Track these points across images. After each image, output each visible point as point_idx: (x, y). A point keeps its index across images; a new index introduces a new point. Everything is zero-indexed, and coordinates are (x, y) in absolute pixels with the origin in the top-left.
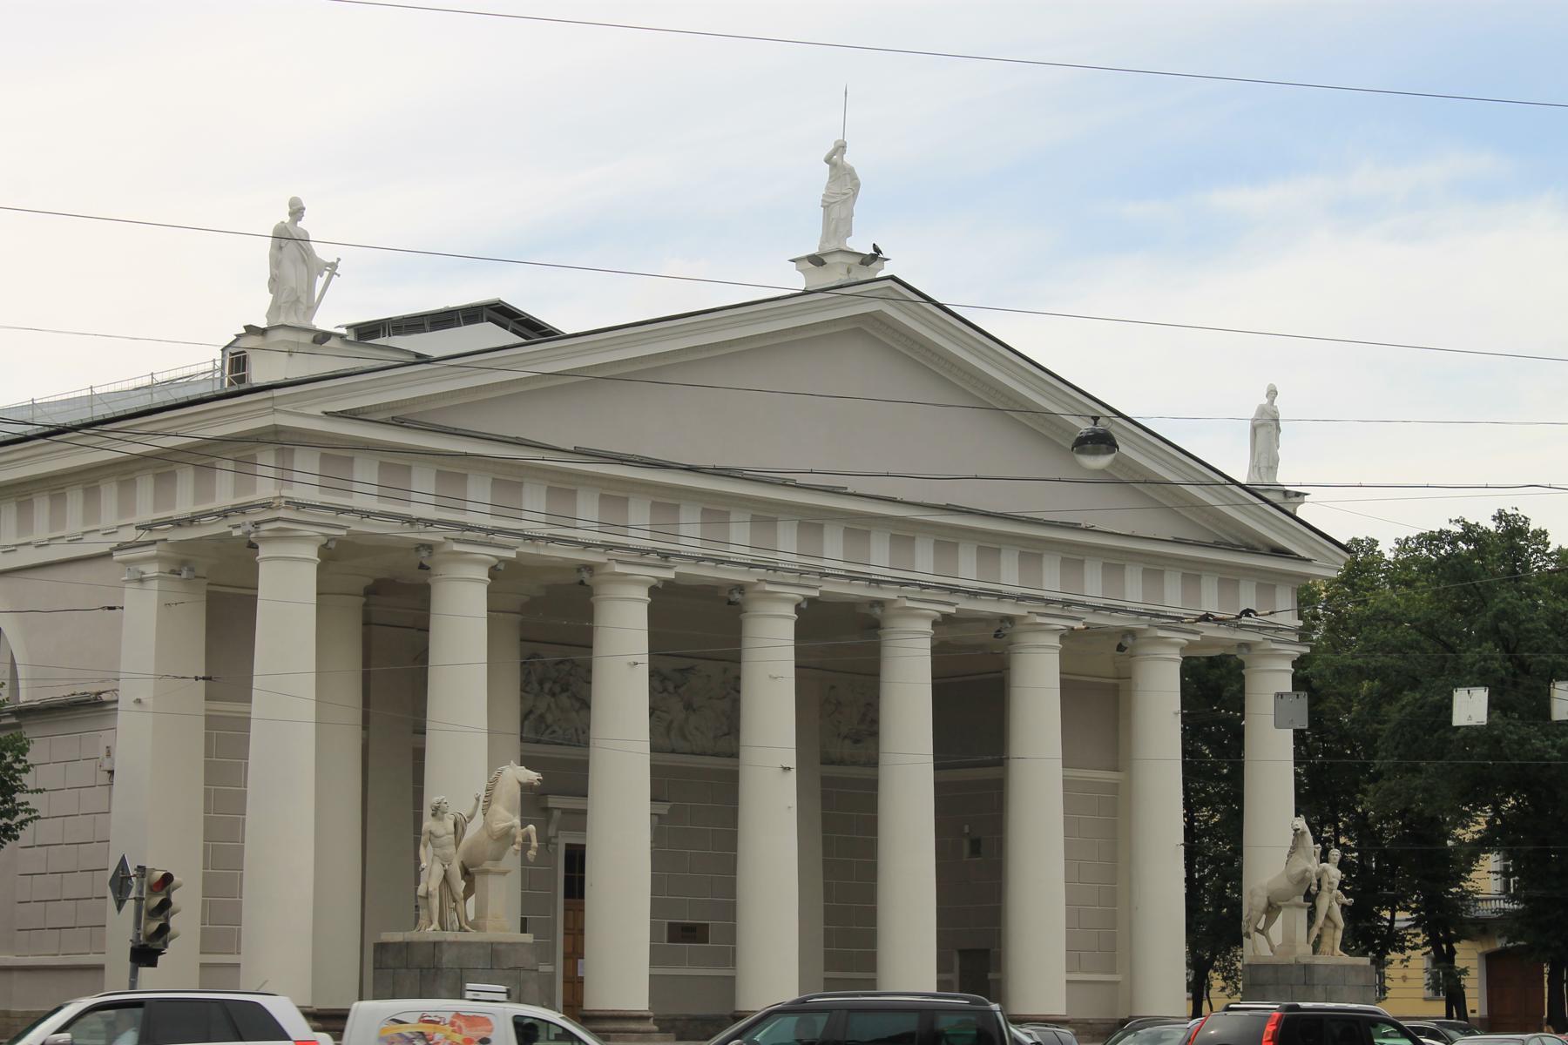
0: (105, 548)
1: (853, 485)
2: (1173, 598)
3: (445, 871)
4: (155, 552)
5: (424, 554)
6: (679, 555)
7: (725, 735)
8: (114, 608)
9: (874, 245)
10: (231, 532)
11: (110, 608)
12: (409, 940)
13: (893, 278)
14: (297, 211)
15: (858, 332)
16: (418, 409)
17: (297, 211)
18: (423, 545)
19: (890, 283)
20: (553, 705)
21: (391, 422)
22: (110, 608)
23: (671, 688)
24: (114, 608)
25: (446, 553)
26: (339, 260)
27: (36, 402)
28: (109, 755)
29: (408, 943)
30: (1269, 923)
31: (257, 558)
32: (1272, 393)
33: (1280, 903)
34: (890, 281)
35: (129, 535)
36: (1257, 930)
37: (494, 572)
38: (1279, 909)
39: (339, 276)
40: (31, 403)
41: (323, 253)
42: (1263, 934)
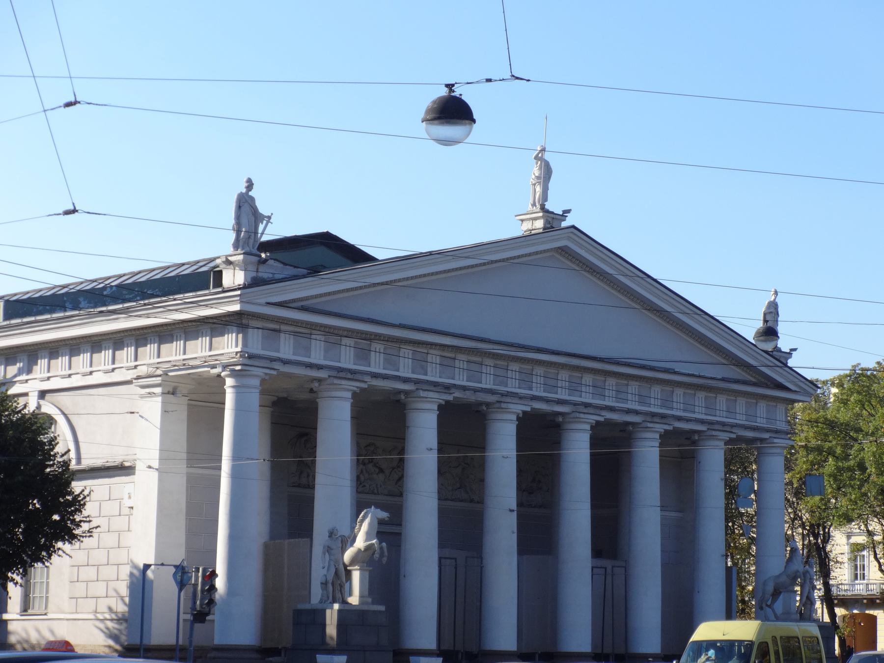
0: (128, 378)
1: (678, 367)
2: (347, 359)
3: (336, 569)
4: (160, 382)
5: (316, 384)
7: (459, 488)
8: (133, 413)
9: (568, 211)
10: (209, 371)
12: (315, 608)
13: (573, 227)
18: (315, 380)
19: (573, 230)
20: (364, 471)
21: (301, 308)
24: (133, 413)
26: (272, 214)
29: (314, 610)
30: (774, 602)
31: (225, 387)
32: (250, 185)
33: (781, 590)
34: (572, 229)
36: (767, 605)
37: (440, 407)
38: (780, 593)
39: (272, 223)
41: (263, 209)
42: (770, 608)
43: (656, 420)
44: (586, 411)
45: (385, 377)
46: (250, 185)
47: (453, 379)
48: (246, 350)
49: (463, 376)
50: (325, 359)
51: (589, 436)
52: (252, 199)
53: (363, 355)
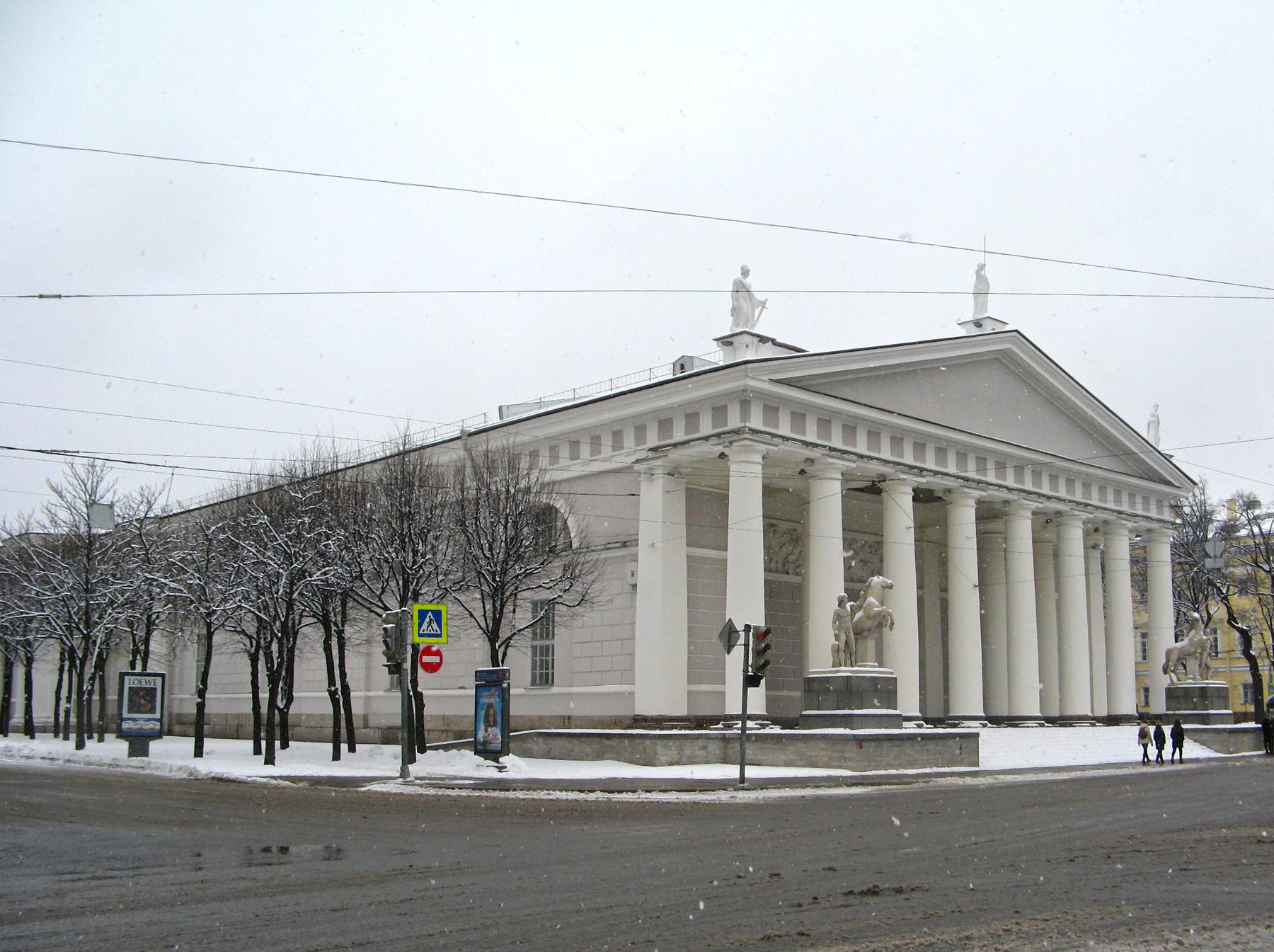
6: (926, 470)
11: (632, 495)
14: (745, 273)
15: (998, 360)
16: (815, 382)
17: (745, 273)
22: (632, 495)
23: (874, 552)
25: (824, 464)
26: (767, 300)
27: (543, 400)
28: (633, 575)
35: (643, 455)
40: (539, 401)
41: (759, 297)
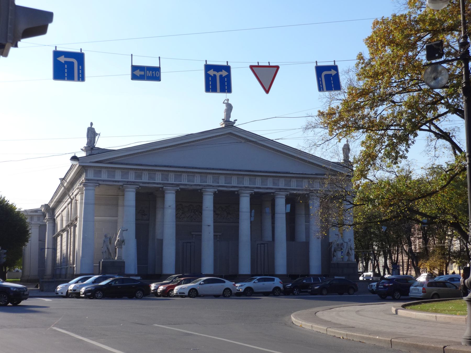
32: (92, 124)
41: (97, 131)
43: (282, 191)
44: (246, 189)
45: (148, 183)
46: (92, 124)
47: (181, 182)
48: (87, 178)
49: (185, 180)
50: (188, 181)
51: (249, 198)
52: (94, 129)
53: (139, 175)
